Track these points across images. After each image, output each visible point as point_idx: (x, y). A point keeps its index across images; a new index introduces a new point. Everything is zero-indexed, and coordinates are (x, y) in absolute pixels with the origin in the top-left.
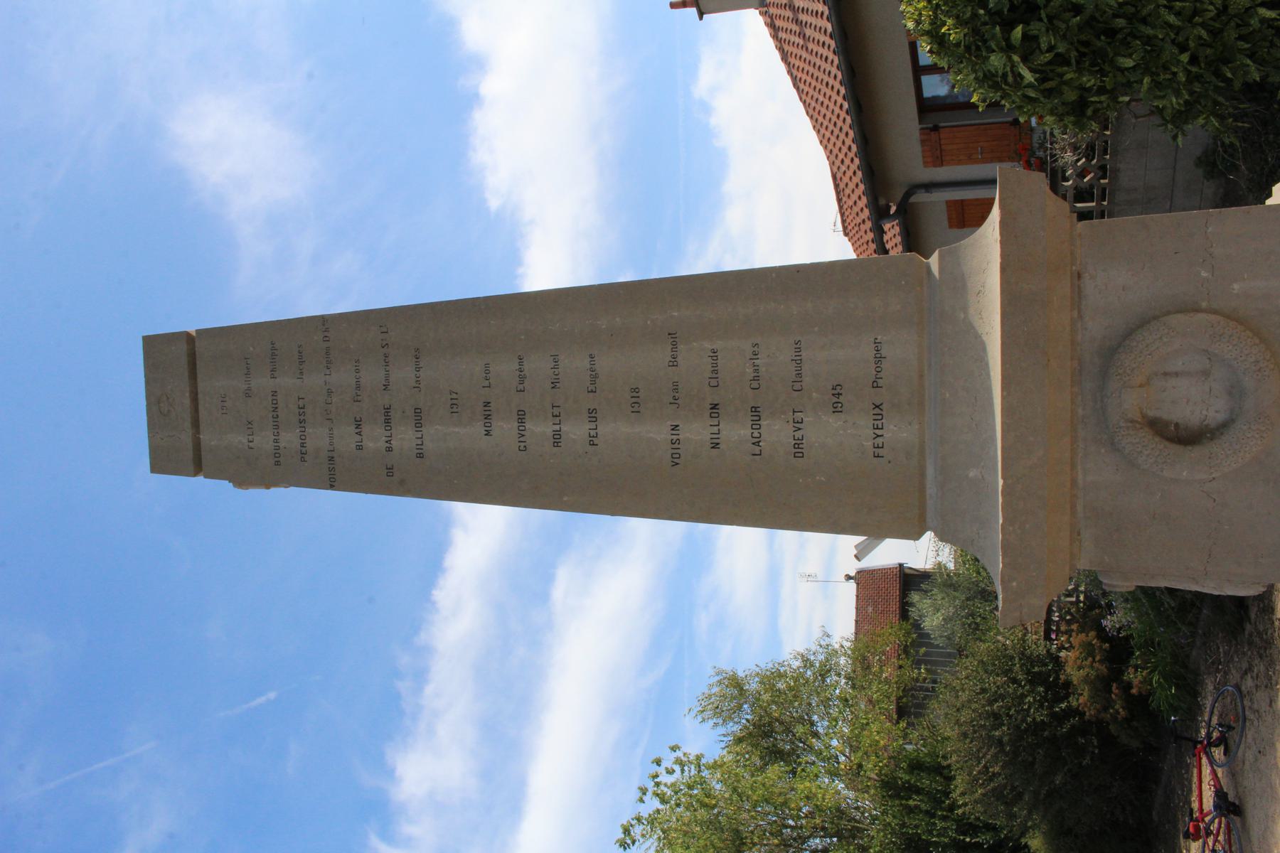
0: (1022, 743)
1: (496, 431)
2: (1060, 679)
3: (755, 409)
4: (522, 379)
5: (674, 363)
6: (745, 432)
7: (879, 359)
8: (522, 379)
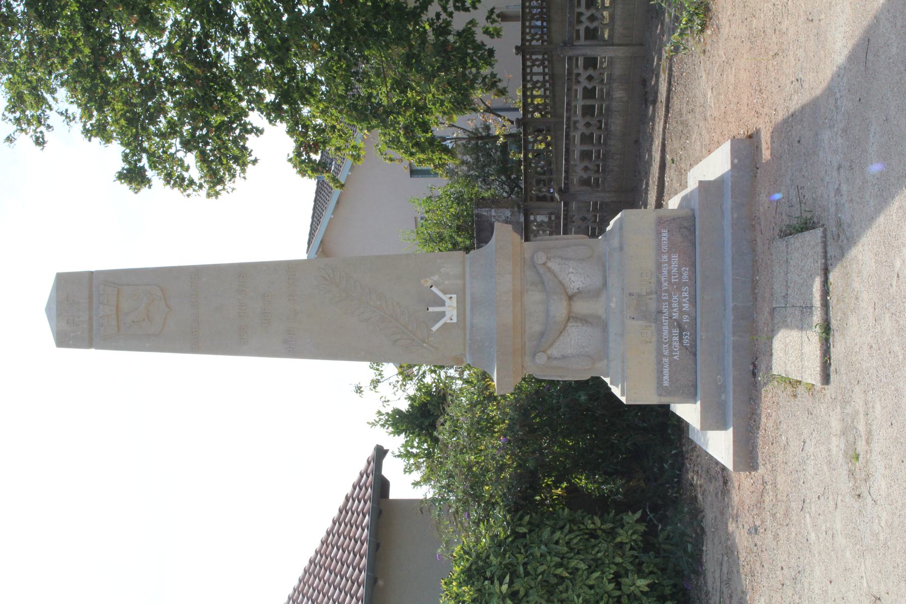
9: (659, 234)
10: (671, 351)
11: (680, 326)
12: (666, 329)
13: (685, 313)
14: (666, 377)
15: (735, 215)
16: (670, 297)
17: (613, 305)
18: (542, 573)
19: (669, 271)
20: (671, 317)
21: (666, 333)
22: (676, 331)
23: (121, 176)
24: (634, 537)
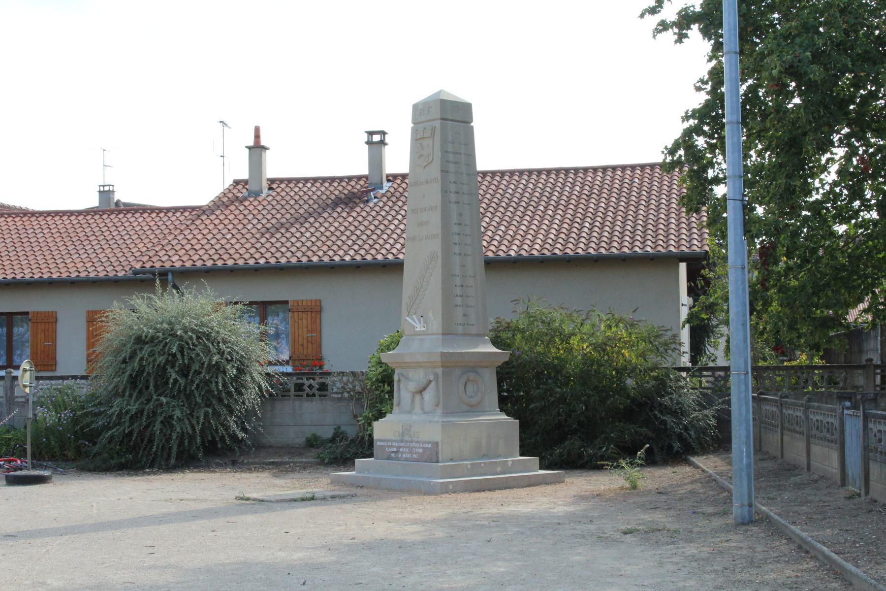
0: (164, 409)
1: (456, 226)
2: (868, 243)
3: (462, 296)
4: (466, 235)
5: (470, 276)
6: (459, 293)
7: (472, 325)
8: (466, 235)
9: (429, 443)
11: (397, 452)
15: (413, 482)
16: (407, 447)
22: (395, 450)
23: (387, 133)
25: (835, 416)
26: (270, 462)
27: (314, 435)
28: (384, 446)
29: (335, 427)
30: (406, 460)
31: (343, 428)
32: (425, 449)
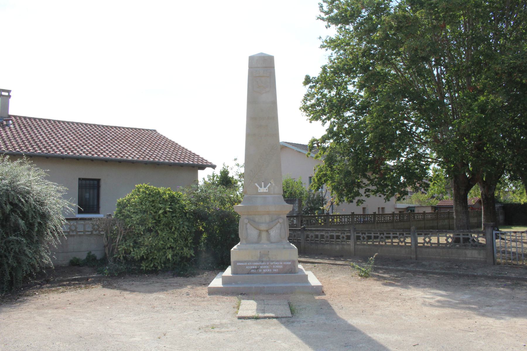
9: (289, 261)
10: (249, 266)
12: (257, 264)
13: (262, 270)
14: (240, 264)
16: (268, 265)
17: (265, 246)
18: (173, 222)
19: (277, 265)
20: (261, 265)
21: (255, 264)
22: (256, 267)
23: (10, 91)
24: (185, 254)
25: (350, 231)
26: (73, 279)
27: (75, 258)
28: (245, 265)
29: (88, 252)
30: (266, 273)
31: (93, 253)
32: (285, 266)
